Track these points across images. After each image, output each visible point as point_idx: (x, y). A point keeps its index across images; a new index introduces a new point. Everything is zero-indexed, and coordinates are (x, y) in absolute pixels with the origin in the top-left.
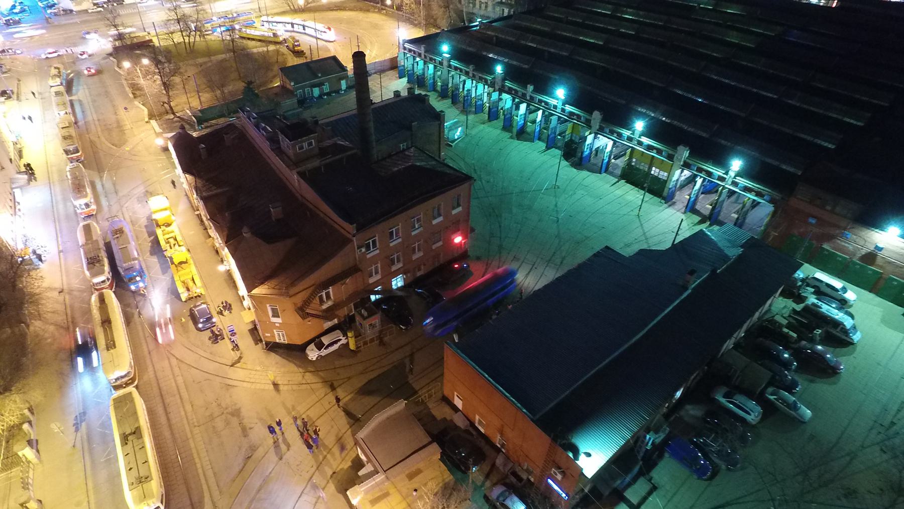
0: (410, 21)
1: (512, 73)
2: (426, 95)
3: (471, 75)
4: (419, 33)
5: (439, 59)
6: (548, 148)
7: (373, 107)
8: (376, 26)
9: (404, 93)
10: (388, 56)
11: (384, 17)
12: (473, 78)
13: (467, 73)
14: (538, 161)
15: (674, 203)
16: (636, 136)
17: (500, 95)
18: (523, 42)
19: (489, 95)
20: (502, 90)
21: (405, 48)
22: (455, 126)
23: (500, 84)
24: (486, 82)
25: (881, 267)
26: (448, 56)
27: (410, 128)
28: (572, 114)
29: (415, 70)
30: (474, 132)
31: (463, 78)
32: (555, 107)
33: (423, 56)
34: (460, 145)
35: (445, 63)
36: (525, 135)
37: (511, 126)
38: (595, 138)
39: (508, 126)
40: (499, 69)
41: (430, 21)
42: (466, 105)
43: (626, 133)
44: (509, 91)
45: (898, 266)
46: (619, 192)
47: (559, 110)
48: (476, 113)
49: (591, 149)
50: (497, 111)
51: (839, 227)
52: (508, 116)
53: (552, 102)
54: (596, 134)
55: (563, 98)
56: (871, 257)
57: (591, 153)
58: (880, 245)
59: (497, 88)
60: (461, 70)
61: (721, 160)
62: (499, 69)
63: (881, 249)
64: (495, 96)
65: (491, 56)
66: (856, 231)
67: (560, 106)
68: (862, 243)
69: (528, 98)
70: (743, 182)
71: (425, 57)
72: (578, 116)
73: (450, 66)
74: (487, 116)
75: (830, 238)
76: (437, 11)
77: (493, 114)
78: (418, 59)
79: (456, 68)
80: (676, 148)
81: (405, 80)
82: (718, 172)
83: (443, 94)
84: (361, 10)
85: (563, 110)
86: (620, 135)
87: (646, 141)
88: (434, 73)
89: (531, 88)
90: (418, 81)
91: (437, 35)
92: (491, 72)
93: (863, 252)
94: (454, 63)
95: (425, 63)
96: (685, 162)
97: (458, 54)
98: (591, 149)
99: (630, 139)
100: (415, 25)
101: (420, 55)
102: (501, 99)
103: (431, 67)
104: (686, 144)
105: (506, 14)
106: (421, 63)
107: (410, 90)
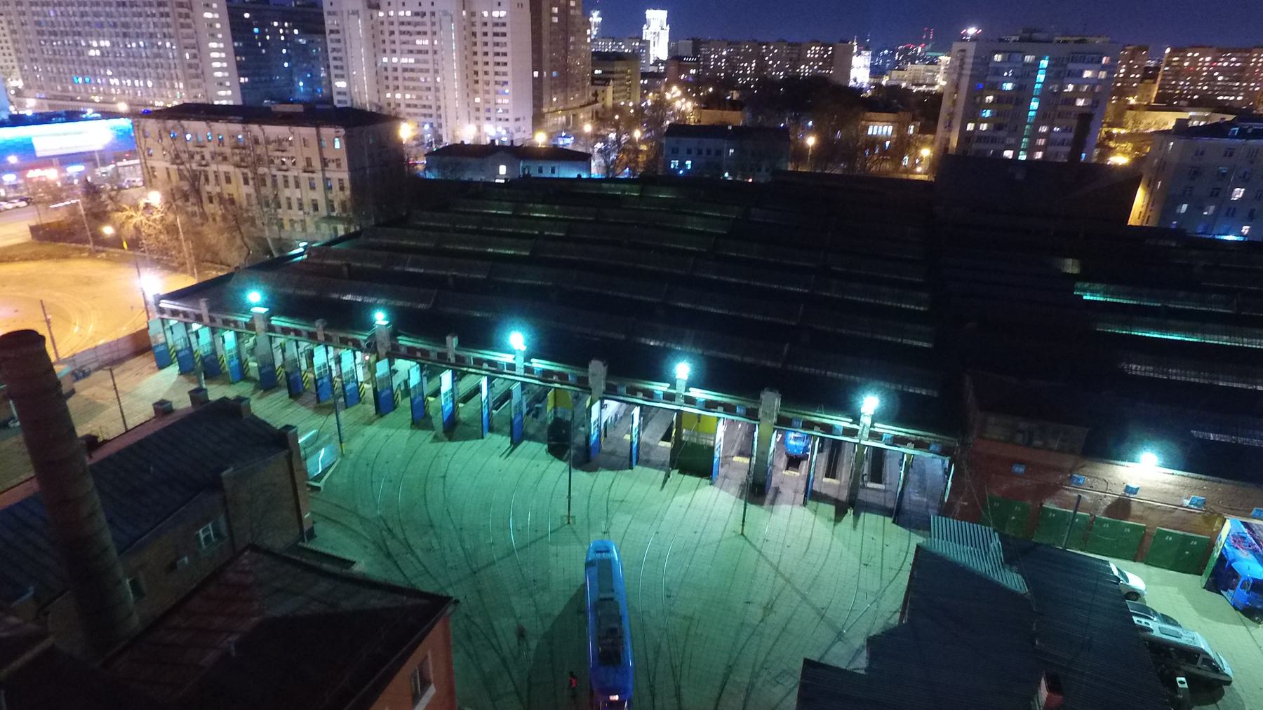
0: (164, 260)
1: (404, 322)
2: (240, 399)
3: (321, 337)
4: (185, 281)
5: (244, 319)
6: (515, 443)
7: (99, 455)
8: (88, 282)
9: (182, 402)
10: (125, 331)
11: (104, 265)
12: (328, 341)
13: (312, 336)
14: (505, 478)
15: (777, 491)
16: (680, 389)
17: (391, 363)
18: (397, 268)
19: (370, 368)
20: (394, 354)
21: (162, 311)
22: (315, 443)
23: (387, 344)
24: (357, 346)
25: (1141, 518)
26: (264, 310)
27: (215, 485)
28: (546, 375)
29: (195, 347)
30: (356, 445)
31: (304, 345)
32: (512, 367)
33: (206, 320)
34: (336, 480)
35: (260, 325)
36: (458, 429)
37: (427, 416)
38: (602, 407)
39: (421, 419)
40: (380, 318)
41: (205, 255)
42: (328, 396)
43: (660, 388)
44: (410, 354)
45: (1165, 511)
46: (682, 499)
47: (520, 370)
48: (347, 406)
49: (599, 427)
50: (392, 394)
51: (1061, 470)
52: (419, 399)
53: (503, 358)
54: (602, 400)
55: (524, 348)
56: (1122, 507)
57: (599, 436)
58: (1133, 485)
59: (382, 351)
60: (297, 333)
61: (842, 403)
62: (380, 318)
63: (1135, 491)
64: (382, 368)
65: (348, 297)
66: (1087, 470)
67: (520, 363)
68: (1103, 487)
69: (453, 360)
70: (888, 430)
71: (212, 320)
72: (563, 377)
73: (271, 328)
74: (371, 409)
75: (1052, 490)
76: (213, 235)
77: (384, 403)
78: (196, 326)
79: (285, 331)
80: (758, 397)
81: (174, 370)
82: (840, 422)
83: (267, 382)
84: (49, 257)
85: (529, 370)
86: (650, 395)
87: (701, 395)
88: (238, 347)
89: (453, 342)
90: (211, 368)
91: (228, 277)
92: (367, 325)
93: (1109, 500)
94: (277, 322)
95: (214, 331)
96: (779, 417)
97: (281, 305)
98: (599, 427)
99: (669, 397)
100: (175, 270)
101: (199, 318)
102: (395, 372)
103: (229, 336)
104: (773, 387)
105: (341, 233)
106: (205, 335)
107: (197, 396)
